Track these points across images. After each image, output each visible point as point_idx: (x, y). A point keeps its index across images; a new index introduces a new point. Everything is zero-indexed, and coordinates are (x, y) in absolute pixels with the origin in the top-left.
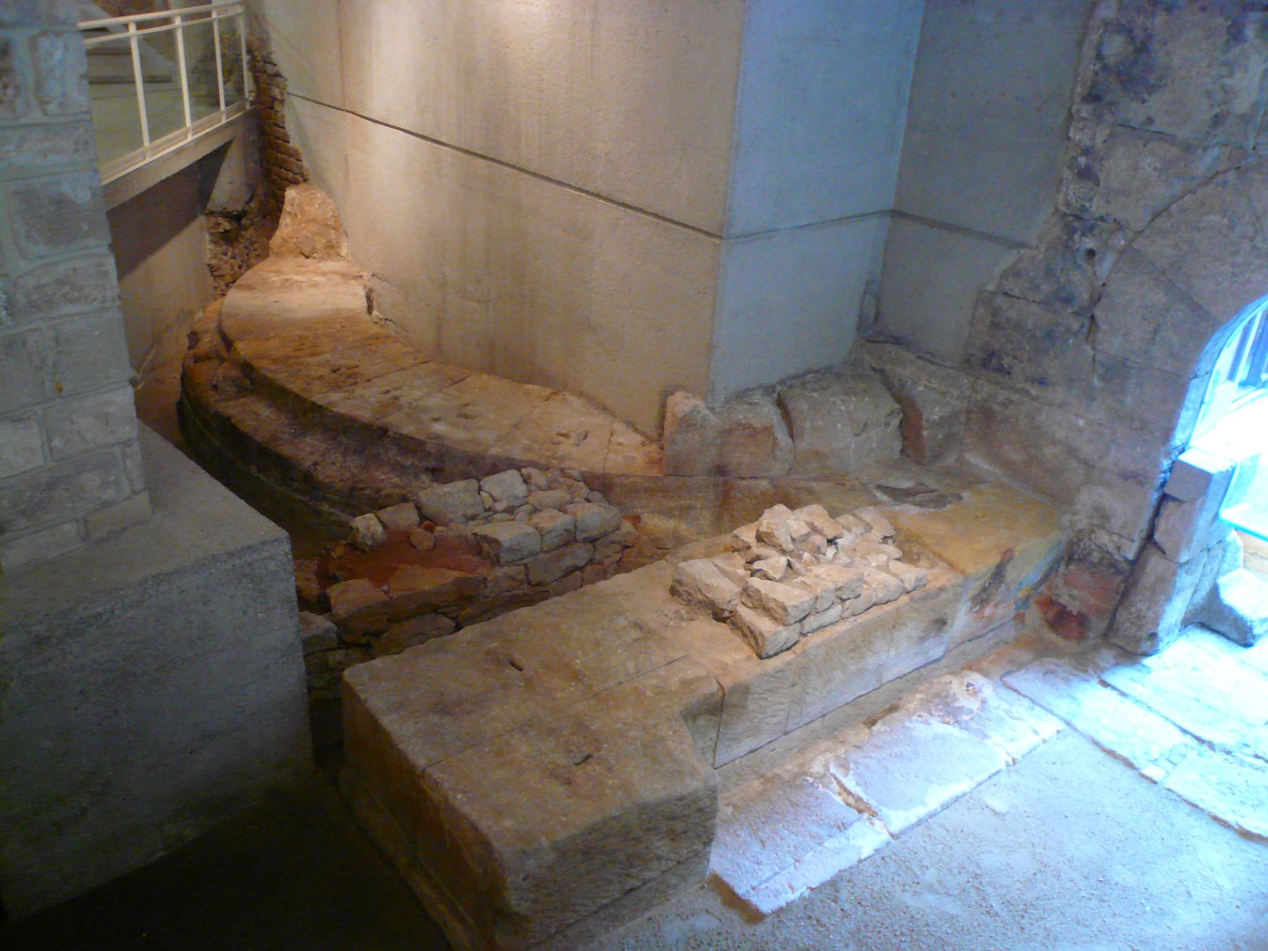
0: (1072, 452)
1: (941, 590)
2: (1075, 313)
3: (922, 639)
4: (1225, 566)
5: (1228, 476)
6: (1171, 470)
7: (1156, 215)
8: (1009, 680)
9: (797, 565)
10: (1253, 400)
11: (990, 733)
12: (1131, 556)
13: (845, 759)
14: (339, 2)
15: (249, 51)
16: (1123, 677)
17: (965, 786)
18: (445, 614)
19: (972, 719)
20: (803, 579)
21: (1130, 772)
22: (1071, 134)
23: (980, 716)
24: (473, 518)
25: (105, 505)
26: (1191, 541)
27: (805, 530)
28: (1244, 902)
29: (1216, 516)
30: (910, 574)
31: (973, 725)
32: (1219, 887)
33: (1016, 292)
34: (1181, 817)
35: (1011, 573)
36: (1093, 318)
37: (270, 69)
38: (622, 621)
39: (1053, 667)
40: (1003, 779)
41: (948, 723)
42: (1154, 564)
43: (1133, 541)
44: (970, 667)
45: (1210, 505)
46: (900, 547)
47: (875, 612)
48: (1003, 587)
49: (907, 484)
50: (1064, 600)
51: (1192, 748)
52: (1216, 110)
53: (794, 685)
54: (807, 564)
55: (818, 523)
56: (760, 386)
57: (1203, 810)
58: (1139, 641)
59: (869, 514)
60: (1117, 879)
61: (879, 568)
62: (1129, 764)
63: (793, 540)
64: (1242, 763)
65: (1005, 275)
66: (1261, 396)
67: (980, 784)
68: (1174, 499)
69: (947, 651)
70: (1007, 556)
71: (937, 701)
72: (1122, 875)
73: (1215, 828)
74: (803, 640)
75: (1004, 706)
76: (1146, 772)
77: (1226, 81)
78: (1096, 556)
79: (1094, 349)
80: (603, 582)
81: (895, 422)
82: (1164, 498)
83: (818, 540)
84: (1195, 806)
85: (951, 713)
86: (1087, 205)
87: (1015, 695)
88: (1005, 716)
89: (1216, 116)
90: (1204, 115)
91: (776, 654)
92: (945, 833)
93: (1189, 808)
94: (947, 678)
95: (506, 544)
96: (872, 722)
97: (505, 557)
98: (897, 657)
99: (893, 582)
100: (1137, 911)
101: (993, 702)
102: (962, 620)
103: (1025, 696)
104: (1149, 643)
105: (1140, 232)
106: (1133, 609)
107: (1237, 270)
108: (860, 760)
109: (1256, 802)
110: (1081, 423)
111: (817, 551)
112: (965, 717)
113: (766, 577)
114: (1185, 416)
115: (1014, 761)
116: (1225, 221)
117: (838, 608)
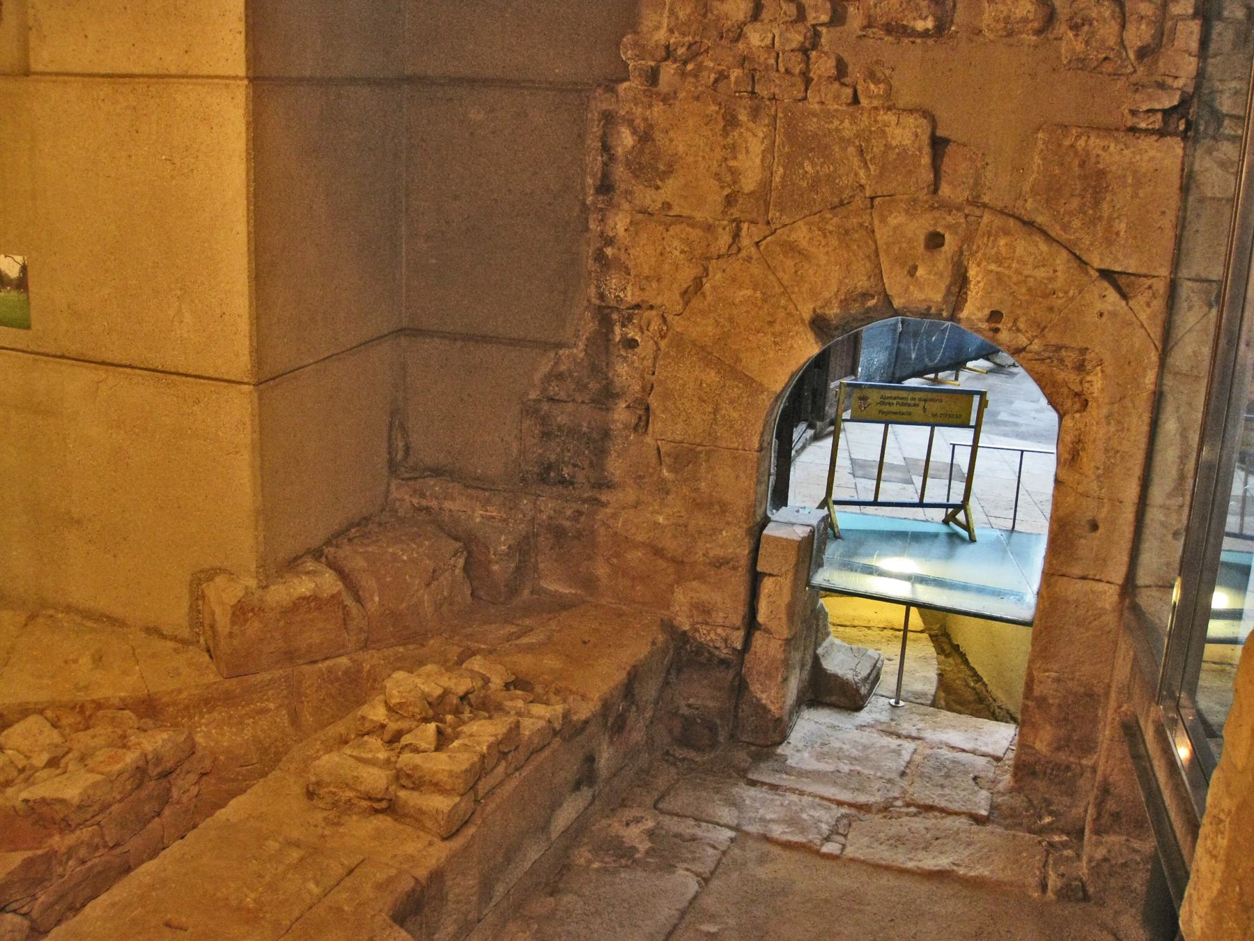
0: (658, 552)
18: (15, 911)
33: (563, 395)
38: (273, 845)
52: (727, 191)
63: (430, 704)
65: (548, 378)
76: (825, 849)
80: (223, 811)
86: (622, 295)
90: (715, 197)
94: (604, 822)
95: (76, 801)
97: (75, 819)
103: (686, 817)
107: (778, 339)
113: (416, 750)
116: (758, 294)
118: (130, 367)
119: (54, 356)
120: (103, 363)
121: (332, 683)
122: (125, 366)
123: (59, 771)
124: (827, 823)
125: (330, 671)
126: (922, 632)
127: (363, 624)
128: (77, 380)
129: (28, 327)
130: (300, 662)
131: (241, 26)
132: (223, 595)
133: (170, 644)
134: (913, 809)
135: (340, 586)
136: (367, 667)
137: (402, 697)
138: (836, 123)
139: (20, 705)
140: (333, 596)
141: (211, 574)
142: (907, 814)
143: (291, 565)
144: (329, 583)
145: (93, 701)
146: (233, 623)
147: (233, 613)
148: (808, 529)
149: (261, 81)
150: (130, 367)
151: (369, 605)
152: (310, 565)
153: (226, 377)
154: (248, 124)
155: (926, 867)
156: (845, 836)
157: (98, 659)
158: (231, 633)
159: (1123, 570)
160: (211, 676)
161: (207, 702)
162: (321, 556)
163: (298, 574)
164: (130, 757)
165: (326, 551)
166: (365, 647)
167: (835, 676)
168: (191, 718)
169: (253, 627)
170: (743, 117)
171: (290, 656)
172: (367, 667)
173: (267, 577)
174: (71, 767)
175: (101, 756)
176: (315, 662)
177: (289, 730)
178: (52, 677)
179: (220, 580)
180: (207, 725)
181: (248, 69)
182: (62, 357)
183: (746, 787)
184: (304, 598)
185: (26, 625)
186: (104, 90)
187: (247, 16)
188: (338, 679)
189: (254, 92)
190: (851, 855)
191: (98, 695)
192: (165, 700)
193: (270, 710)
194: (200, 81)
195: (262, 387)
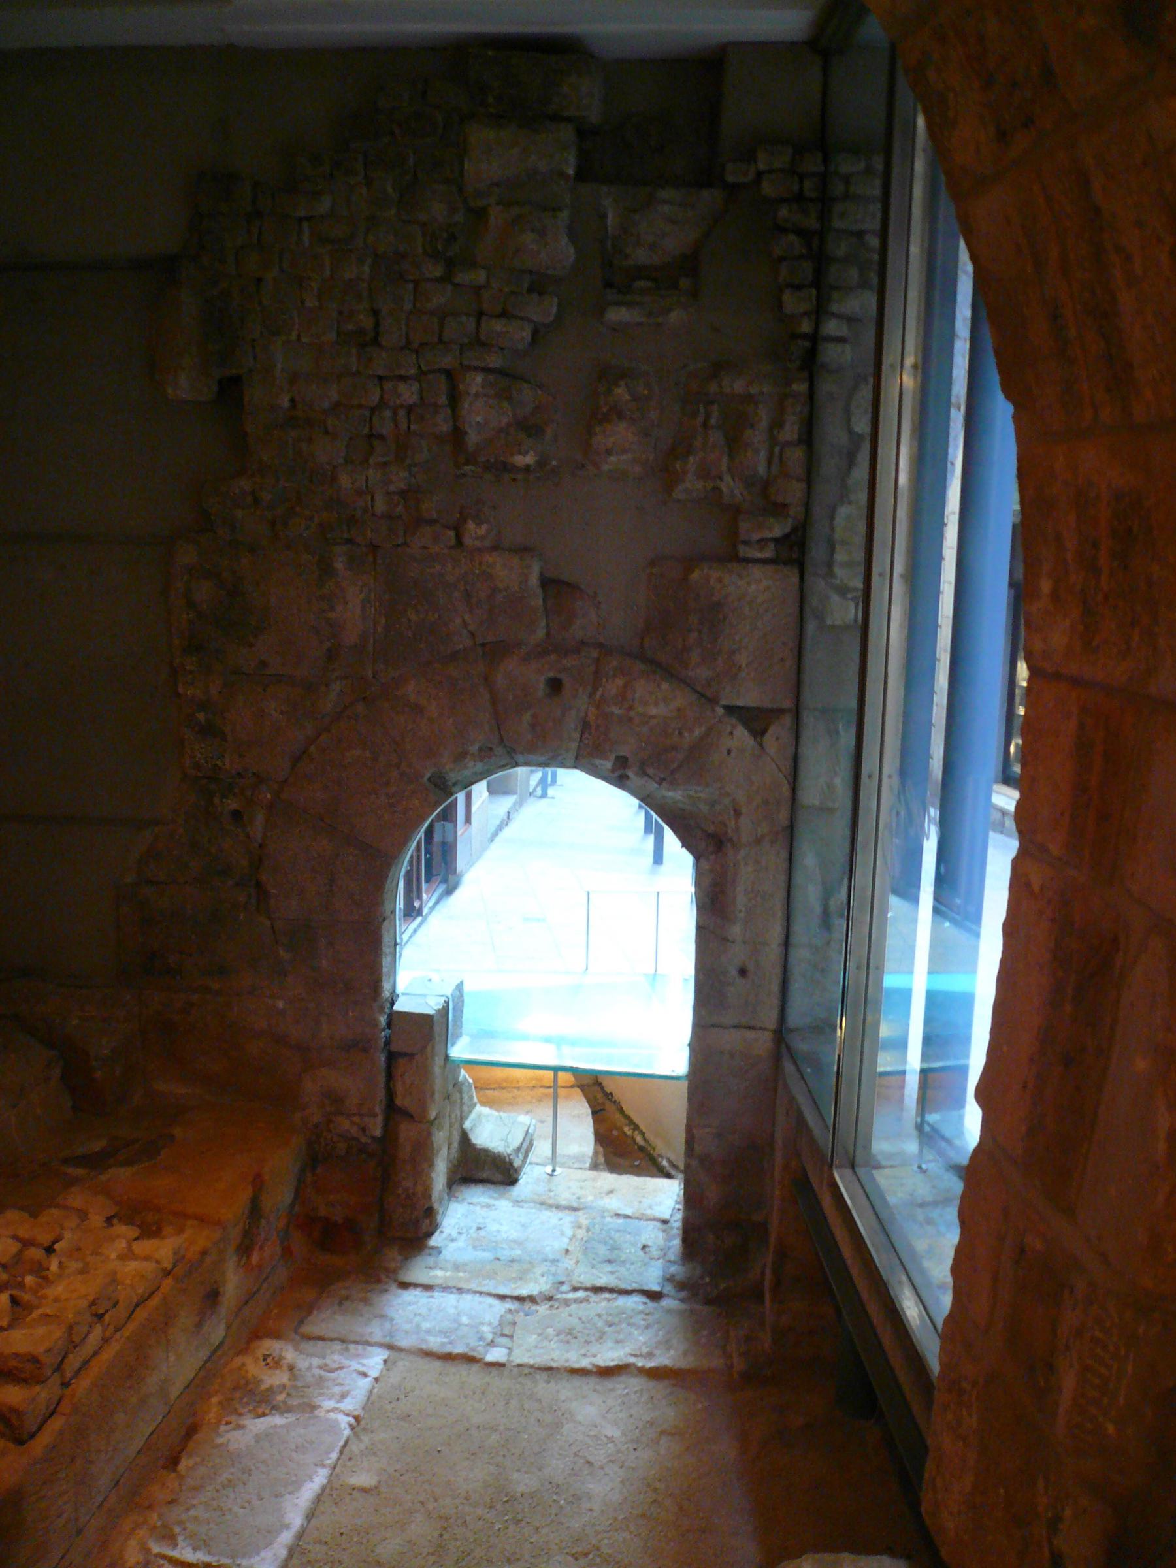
1: (204, 1253)
2: (237, 884)
3: (199, 1325)
4: (465, 1108)
5: (444, 1011)
6: (389, 1025)
7: (297, 759)
8: (307, 1329)
9: (26, 1297)
10: (415, 931)
11: (317, 1401)
12: (378, 1132)
13: (164, 1526)
16: (418, 1271)
17: (320, 1478)
19: (289, 1395)
20: (40, 1311)
21: (475, 1367)
22: (181, 690)
23: (295, 1387)
26: (433, 1094)
27: (14, 1247)
28: (637, 1441)
29: (447, 1057)
30: (164, 1249)
31: (294, 1402)
32: (611, 1439)
34: (543, 1388)
35: (267, 1204)
36: (258, 885)
39: (343, 1292)
40: (354, 1447)
41: (264, 1415)
42: (406, 1132)
43: (375, 1116)
44: (257, 1335)
45: (439, 1048)
46: (130, 1221)
47: (141, 1314)
48: (263, 1221)
49: (98, 1145)
50: (323, 1212)
51: (517, 1311)
52: (327, 645)
53: (73, 1460)
54: (34, 1292)
55: (23, 1232)
57: (558, 1369)
58: (417, 1223)
59: (76, 1198)
60: (521, 1489)
61: (122, 1258)
62: (469, 1359)
64: (567, 1303)
66: (420, 925)
67: (334, 1468)
68: (405, 1054)
69: (228, 1327)
70: (258, 1183)
71: (238, 1394)
72: (523, 1482)
73: (577, 1381)
74: (67, 1392)
75: (316, 1361)
76: (489, 1358)
77: (331, 615)
78: (342, 1146)
79: (270, 918)
81: (57, 1072)
82: (392, 1057)
83: (36, 1253)
84: (550, 1369)
85: (263, 1401)
86: (219, 763)
87: (320, 1343)
88: (322, 1373)
89: (329, 650)
91: (40, 1428)
92: (324, 1548)
93: (545, 1375)
94: (238, 1361)
96: (173, 1462)
98: (177, 1365)
99: (150, 1266)
100: (553, 1511)
101: (302, 1363)
102: (233, 1283)
103: (331, 1340)
104: (427, 1222)
105: (286, 781)
106: (400, 1191)
108: (184, 1517)
109: (598, 1335)
110: (281, 1004)
111: (39, 1269)
112: (281, 1397)
114: (386, 962)
115: (357, 1418)
116: (368, 753)
117: (98, 1330)
124: (490, 1324)
126: (572, 1087)
134: (581, 1294)
138: (438, 567)
142: (575, 1301)
148: (442, 1000)
155: (602, 1364)
156: (511, 1337)
159: (774, 1014)
167: (486, 1151)
170: (339, 565)
183: (400, 1291)
190: (519, 1361)
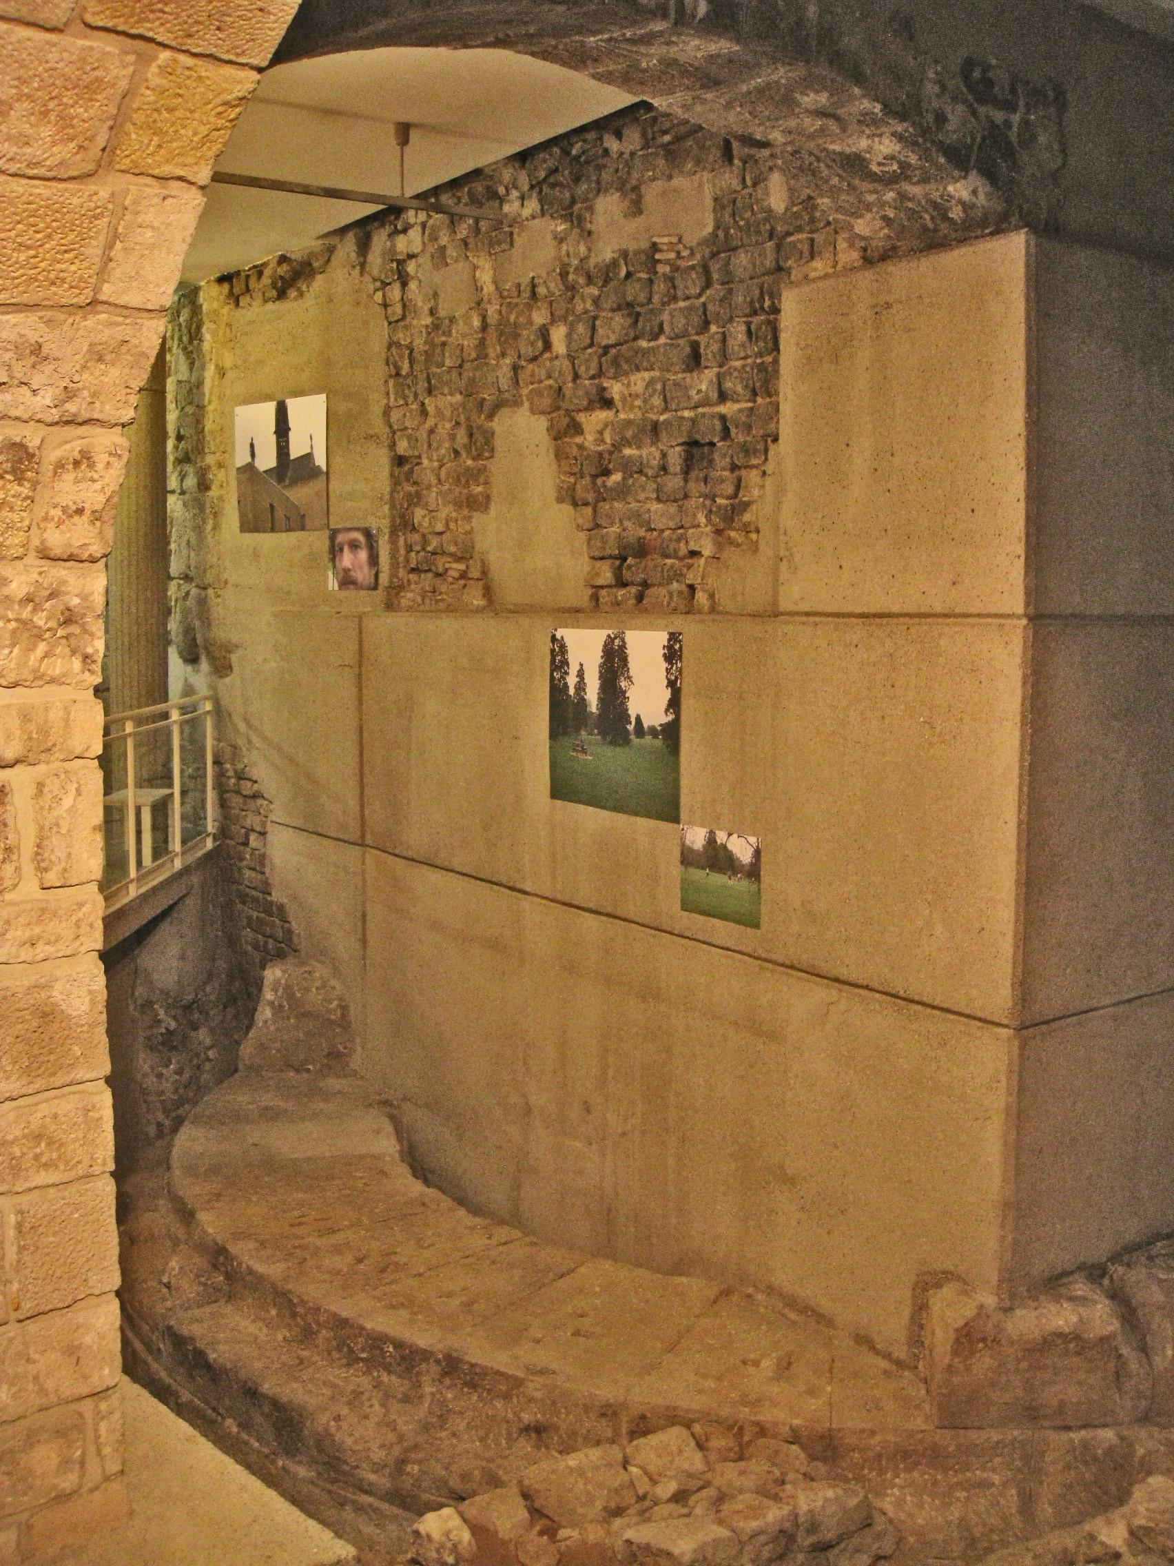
14: (5, 417)
15: (217, 762)
24: (618, 1512)
25: (63, 1498)
37: (247, 788)
56: (1081, 1268)
118: (867, 988)
119: (783, 965)
120: (837, 980)
121: (1086, 1463)
122: (861, 987)
123: (685, 1511)
125: (1085, 1445)
127: (1145, 1386)
128: (801, 1000)
129: (757, 926)
130: (1047, 1424)
131: (1020, 549)
132: (950, 1310)
133: (884, 1364)
135: (1114, 1326)
136: (1141, 1451)
137: (1150, 1519)
139: (667, 1408)
140: (1102, 1340)
141: (942, 1278)
143: (1053, 1284)
144: (1100, 1317)
145: (757, 1424)
146: (955, 1353)
147: (957, 1341)
149: (1042, 618)
150: (867, 988)
151: (1157, 1360)
152: (1080, 1288)
153: (979, 1015)
154: (1025, 678)
157: (785, 1367)
158: (950, 1366)
160: (919, 1421)
161: (907, 1455)
162: (1103, 1276)
163: (1057, 1298)
164: (774, 1514)
165: (1111, 1268)
166: (1145, 1419)
168: (882, 1472)
169: (984, 1363)
171: (1032, 1414)
172: (1141, 1451)
173: (1013, 1296)
174: (698, 1511)
175: (744, 1500)
176: (1068, 1428)
177: (1017, 1521)
178: (719, 1379)
179: (948, 1291)
180: (902, 1487)
181: (1027, 605)
182: (792, 967)
184: (1060, 1335)
185: (715, 1302)
186: (858, 632)
187: (1028, 535)
188: (1095, 1459)
189: (1036, 633)
191: (767, 1415)
192: (853, 1440)
193: (993, 1484)
194: (969, 620)
195: (1024, 1032)
